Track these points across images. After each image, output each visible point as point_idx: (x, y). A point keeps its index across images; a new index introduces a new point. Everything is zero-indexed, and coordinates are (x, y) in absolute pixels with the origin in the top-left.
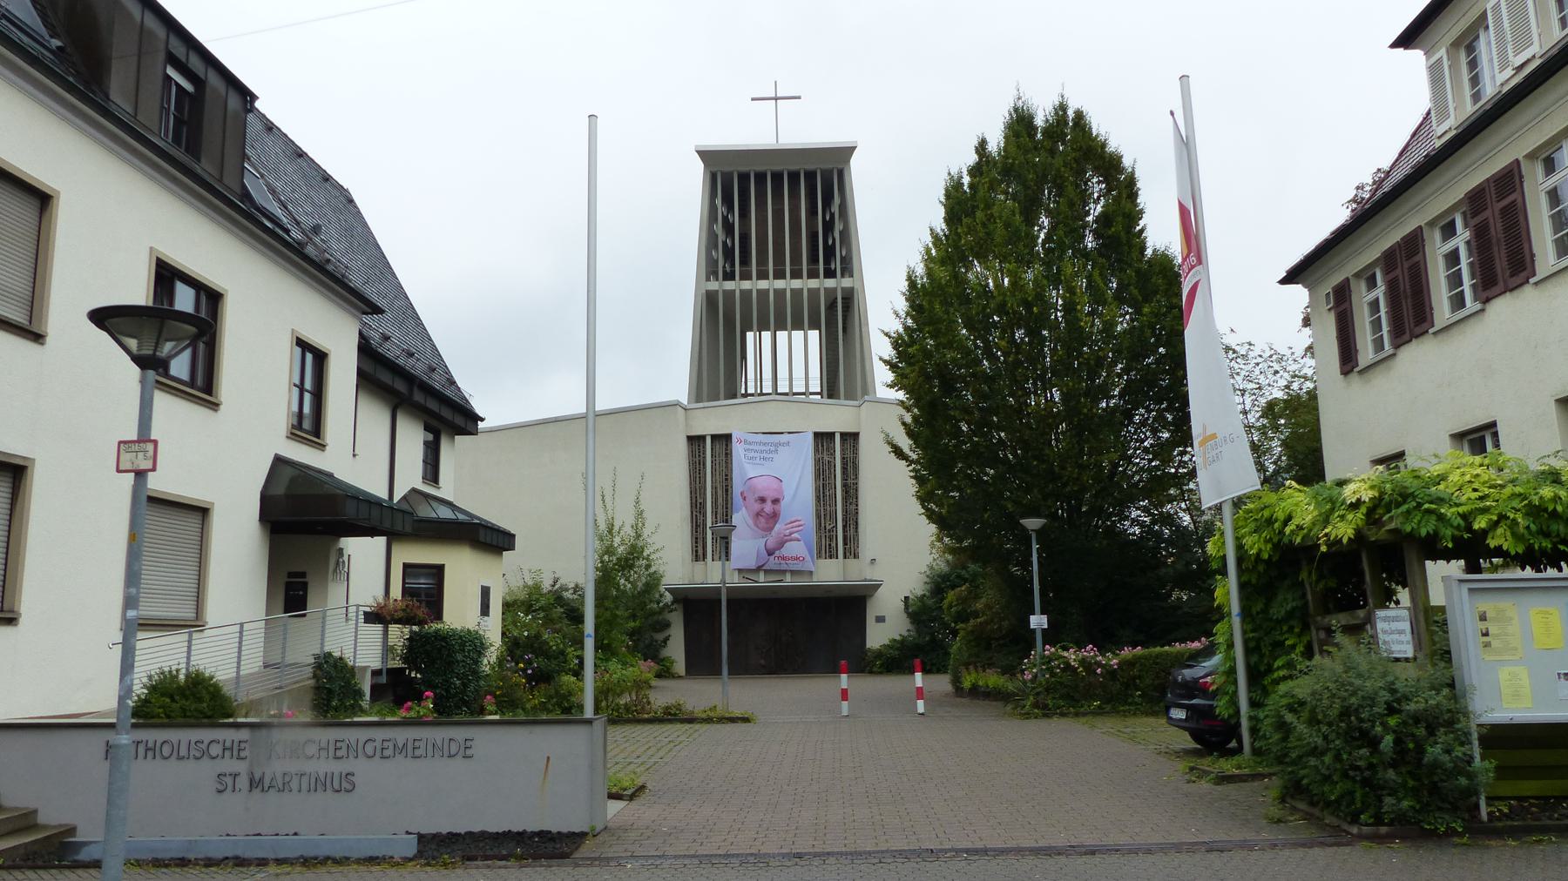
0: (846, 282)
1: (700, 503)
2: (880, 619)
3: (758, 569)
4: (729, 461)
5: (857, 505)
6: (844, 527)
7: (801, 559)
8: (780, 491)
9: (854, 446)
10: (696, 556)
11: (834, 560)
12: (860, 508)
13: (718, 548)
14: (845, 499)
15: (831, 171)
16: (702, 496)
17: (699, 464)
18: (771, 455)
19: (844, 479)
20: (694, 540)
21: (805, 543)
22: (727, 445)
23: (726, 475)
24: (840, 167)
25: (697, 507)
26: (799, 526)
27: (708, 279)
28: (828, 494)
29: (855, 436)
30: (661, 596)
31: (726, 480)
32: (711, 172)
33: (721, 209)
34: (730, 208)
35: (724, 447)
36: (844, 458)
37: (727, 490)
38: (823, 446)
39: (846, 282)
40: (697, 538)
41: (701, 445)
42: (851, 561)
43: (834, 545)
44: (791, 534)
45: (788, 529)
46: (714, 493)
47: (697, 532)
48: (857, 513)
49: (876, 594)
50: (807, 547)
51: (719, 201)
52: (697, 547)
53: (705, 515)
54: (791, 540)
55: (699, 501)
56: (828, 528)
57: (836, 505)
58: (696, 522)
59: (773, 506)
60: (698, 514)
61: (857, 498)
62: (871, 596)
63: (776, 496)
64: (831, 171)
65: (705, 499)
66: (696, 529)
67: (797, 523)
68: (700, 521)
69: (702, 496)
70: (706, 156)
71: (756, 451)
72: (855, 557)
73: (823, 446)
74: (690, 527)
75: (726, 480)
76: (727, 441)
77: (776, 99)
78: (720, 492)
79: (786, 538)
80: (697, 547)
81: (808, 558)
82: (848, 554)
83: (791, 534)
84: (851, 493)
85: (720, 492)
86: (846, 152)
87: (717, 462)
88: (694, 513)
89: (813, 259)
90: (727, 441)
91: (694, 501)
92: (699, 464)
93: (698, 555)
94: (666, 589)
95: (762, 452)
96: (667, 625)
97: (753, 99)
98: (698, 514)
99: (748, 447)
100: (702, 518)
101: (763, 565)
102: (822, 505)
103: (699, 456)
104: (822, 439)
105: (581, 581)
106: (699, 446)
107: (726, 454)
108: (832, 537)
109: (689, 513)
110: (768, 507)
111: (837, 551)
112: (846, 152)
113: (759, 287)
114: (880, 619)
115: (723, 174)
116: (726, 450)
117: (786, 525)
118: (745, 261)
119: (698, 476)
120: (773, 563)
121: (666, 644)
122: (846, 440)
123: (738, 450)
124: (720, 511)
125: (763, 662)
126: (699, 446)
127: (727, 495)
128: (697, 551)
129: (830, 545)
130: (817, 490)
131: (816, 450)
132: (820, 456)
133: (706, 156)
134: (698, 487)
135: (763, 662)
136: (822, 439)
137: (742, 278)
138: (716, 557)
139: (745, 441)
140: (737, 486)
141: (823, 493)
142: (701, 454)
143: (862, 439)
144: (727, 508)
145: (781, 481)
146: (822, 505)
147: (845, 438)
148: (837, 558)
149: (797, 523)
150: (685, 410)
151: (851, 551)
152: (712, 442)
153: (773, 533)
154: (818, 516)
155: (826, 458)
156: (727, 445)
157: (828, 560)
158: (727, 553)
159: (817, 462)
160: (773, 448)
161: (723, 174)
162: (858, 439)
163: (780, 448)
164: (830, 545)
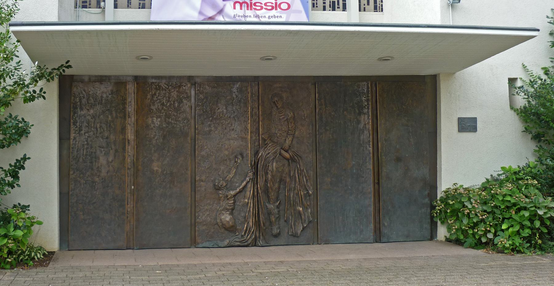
72: (376, 9)
121: (15, 176)
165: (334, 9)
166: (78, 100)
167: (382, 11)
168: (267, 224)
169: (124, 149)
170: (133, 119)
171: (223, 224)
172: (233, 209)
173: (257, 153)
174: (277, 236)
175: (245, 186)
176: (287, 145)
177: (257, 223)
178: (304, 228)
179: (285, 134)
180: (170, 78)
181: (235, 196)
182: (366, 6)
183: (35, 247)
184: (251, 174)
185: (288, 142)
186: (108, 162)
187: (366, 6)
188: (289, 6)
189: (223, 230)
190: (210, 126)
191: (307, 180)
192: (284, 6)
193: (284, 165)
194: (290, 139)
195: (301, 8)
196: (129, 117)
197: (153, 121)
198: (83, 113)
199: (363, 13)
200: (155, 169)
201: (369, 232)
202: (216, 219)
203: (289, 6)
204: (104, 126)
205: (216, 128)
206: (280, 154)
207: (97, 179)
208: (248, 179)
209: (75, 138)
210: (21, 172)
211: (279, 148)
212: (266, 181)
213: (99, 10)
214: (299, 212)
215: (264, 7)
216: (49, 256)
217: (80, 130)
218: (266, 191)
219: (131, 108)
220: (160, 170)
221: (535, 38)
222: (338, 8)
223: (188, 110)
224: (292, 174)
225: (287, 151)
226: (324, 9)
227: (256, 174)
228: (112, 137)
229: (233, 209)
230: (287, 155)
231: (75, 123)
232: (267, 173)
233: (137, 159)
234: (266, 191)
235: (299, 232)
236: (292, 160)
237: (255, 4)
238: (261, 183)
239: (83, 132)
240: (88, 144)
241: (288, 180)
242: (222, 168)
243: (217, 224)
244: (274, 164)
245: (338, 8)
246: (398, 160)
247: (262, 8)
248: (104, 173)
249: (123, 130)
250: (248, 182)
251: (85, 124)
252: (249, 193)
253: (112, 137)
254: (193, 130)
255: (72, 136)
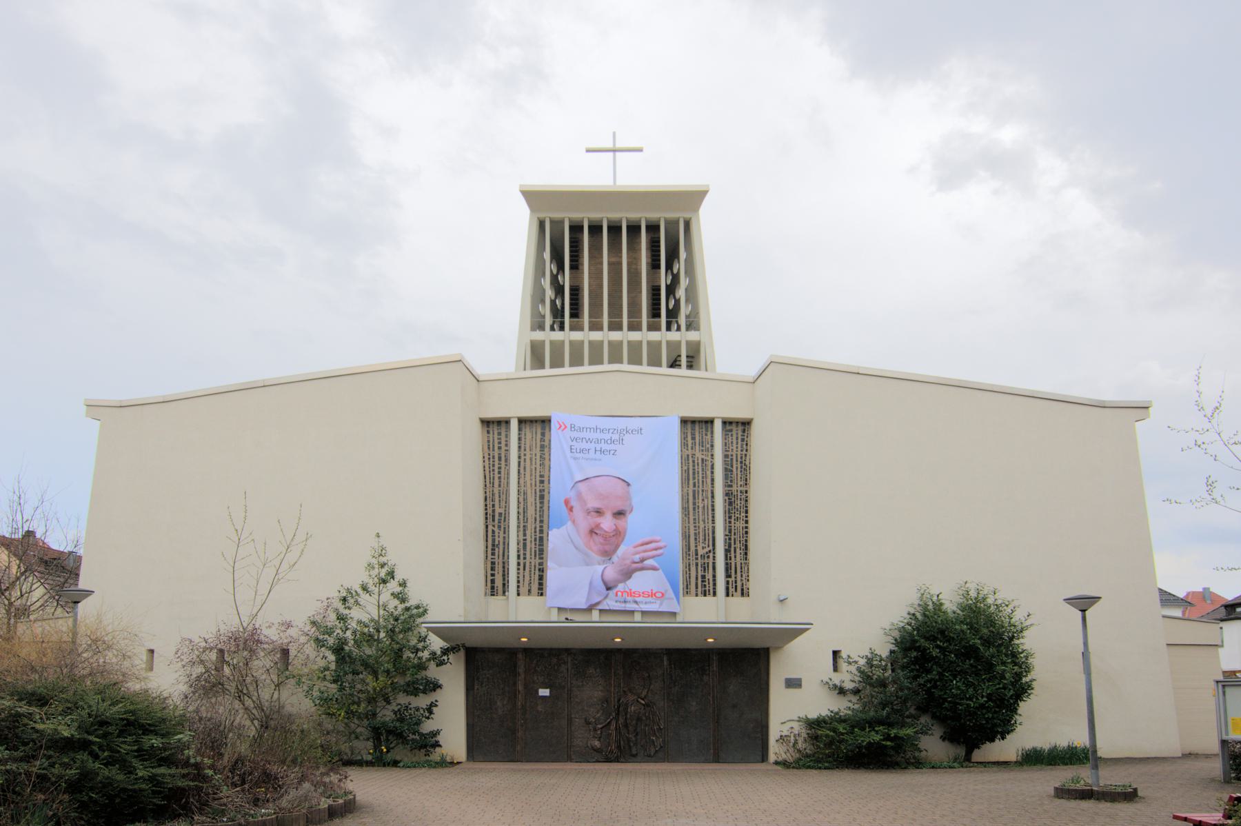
0: (692, 336)
1: (500, 514)
2: (793, 683)
3: (589, 609)
4: (546, 456)
5: (747, 522)
6: (727, 551)
7: (659, 595)
8: (627, 497)
9: (743, 440)
10: (493, 588)
11: (710, 599)
12: (751, 525)
13: (527, 578)
14: (729, 515)
15: (677, 222)
16: (503, 504)
17: (500, 459)
18: (612, 447)
19: (728, 484)
20: (489, 566)
21: (663, 571)
22: (543, 434)
23: (541, 476)
24: (687, 216)
25: (493, 518)
26: (656, 549)
27: (533, 329)
28: (701, 505)
29: (746, 424)
30: (423, 639)
31: (542, 482)
32: (538, 218)
33: (550, 267)
34: (561, 267)
35: (539, 436)
36: (726, 456)
37: (542, 497)
38: (693, 438)
39: (692, 336)
40: (493, 563)
41: (503, 434)
42: (737, 600)
43: (709, 576)
44: (642, 560)
45: (638, 553)
46: (521, 500)
47: (493, 554)
48: (747, 533)
49: (785, 647)
50: (668, 580)
51: (547, 255)
52: (493, 575)
53: (506, 531)
54: (642, 569)
55: (498, 510)
56: (701, 552)
57: (713, 521)
58: (494, 540)
59: (615, 521)
60: (496, 529)
61: (747, 512)
62: (779, 648)
63: (619, 505)
64: (677, 222)
65: (507, 507)
66: (493, 550)
67: (653, 545)
68: (499, 539)
69: (503, 504)
70: (533, 197)
71: (589, 441)
72: (742, 594)
73: (693, 438)
74: (483, 548)
75: (542, 482)
76: (543, 428)
77: (614, 151)
78: (531, 499)
79: (635, 566)
80: (493, 575)
81: (671, 594)
82: (731, 590)
83: (642, 560)
84: (738, 505)
85: (531, 499)
86: (695, 197)
87: (528, 458)
88: (490, 528)
89: (655, 313)
90: (543, 428)
91: (490, 511)
92: (500, 459)
93: (496, 586)
94: (429, 629)
95: (599, 441)
96: (435, 686)
97: (588, 151)
98: (496, 529)
99: (575, 434)
100: (502, 535)
101: (598, 603)
102: (692, 521)
103: (500, 448)
104: (693, 429)
105: (1226, 797)
106: (499, 434)
107: (542, 447)
108: (707, 565)
109: (482, 527)
110: (607, 523)
111: (715, 584)
112: (695, 197)
113: (591, 339)
114: (793, 683)
115: (552, 222)
116: (542, 440)
117: (635, 547)
118: (576, 313)
119: (497, 475)
120: (611, 603)
121: (431, 712)
122: (731, 431)
123: (558, 438)
124: (530, 526)
125: (597, 743)
126: (499, 434)
127: (542, 503)
128: (493, 581)
129: (703, 577)
130: (685, 500)
131: (684, 444)
132: (690, 452)
133: (533, 197)
134: (496, 492)
135: (597, 743)
136: (693, 429)
137: (572, 328)
138: (524, 590)
139: (573, 427)
140: (558, 490)
141: (694, 504)
142: (503, 445)
143: (755, 428)
144: (541, 521)
145: (629, 485)
146: (692, 521)
147: (728, 427)
148: (715, 594)
149: (653, 545)
150: (478, 381)
151: (738, 586)
152: (520, 429)
153: (615, 558)
154: (686, 536)
155: (699, 455)
156: (543, 434)
157: (701, 599)
158: (541, 584)
159: (686, 460)
160: (616, 437)
161: (552, 222)
162: (749, 429)
163: (627, 437)
164: (703, 577)
165: (705, 595)
166: (480, 664)
167: (748, 596)
168: (627, 747)
169: (515, 697)
170: (523, 676)
171: (592, 747)
172: (600, 737)
173: (619, 700)
174: (635, 756)
175: (609, 723)
176: (643, 696)
177: (619, 747)
178: (656, 751)
179: (642, 688)
180: (551, 649)
181: (602, 728)
182: (734, 593)
183: (19, 625)
184: (614, 714)
185: (644, 693)
186: (503, 705)
187: (734, 593)
188: (663, 595)
189: (592, 751)
190: (582, 682)
191: (659, 719)
192: (659, 595)
193: (640, 709)
194: (646, 691)
195: (673, 595)
196: (519, 675)
197: (538, 679)
198: (485, 672)
199: (730, 598)
200: (540, 710)
201: (759, 758)
202: (587, 743)
203: (663, 595)
204: (500, 681)
205: (587, 684)
206: (638, 701)
207: (495, 716)
208: (611, 717)
209: (478, 689)
210: (434, 709)
211: (636, 697)
212: (626, 719)
213: (504, 597)
214: (653, 740)
215: (642, 595)
216: (447, 764)
217: (482, 684)
218: (626, 726)
219: (521, 670)
220: (543, 711)
221: (808, 632)
222: (709, 594)
223: (565, 671)
224: (647, 714)
225: (643, 699)
226: (697, 595)
227: (618, 714)
228: (507, 689)
229: (600, 737)
230: (643, 702)
231: (478, 679)
232: (626, 714)
233: (526, 703)
234: (626, 726)
235: (652, 754)
236: (647, 705)
237: (634, 593)
238: (621, 720)
239: (484, 685)
240: (488, 693)
241: (644, 718)
242: (592, 709)
243: (588, 746)
244: (633, 708)
245: (709, 594)
246: (734, 706)
247: (640, 595)
248: (500, 712)
249: (515, 684)
250: (612, 720)
251: (485, 680)
252: (613, 726)
253: (507, 689)
254: (569, 684)
255: (476, 687)
